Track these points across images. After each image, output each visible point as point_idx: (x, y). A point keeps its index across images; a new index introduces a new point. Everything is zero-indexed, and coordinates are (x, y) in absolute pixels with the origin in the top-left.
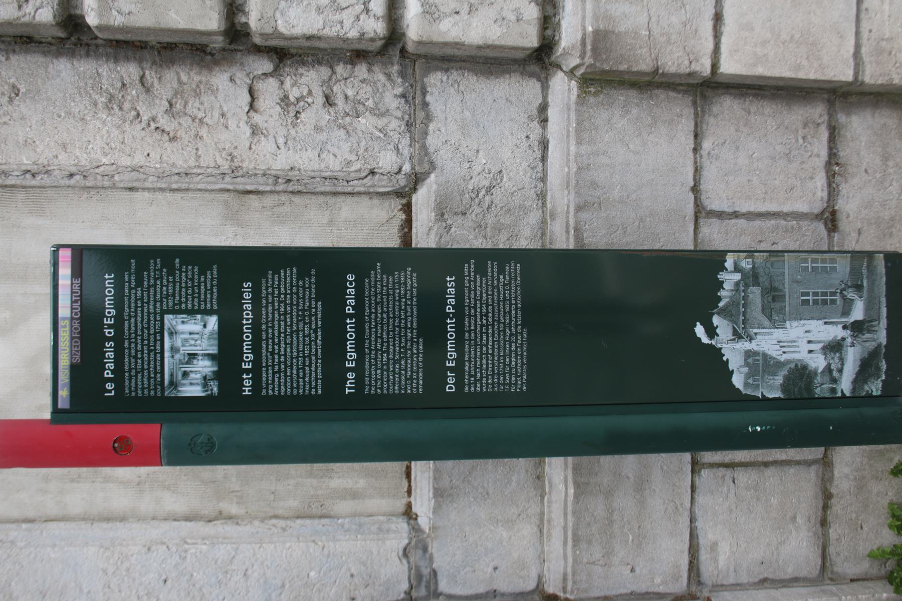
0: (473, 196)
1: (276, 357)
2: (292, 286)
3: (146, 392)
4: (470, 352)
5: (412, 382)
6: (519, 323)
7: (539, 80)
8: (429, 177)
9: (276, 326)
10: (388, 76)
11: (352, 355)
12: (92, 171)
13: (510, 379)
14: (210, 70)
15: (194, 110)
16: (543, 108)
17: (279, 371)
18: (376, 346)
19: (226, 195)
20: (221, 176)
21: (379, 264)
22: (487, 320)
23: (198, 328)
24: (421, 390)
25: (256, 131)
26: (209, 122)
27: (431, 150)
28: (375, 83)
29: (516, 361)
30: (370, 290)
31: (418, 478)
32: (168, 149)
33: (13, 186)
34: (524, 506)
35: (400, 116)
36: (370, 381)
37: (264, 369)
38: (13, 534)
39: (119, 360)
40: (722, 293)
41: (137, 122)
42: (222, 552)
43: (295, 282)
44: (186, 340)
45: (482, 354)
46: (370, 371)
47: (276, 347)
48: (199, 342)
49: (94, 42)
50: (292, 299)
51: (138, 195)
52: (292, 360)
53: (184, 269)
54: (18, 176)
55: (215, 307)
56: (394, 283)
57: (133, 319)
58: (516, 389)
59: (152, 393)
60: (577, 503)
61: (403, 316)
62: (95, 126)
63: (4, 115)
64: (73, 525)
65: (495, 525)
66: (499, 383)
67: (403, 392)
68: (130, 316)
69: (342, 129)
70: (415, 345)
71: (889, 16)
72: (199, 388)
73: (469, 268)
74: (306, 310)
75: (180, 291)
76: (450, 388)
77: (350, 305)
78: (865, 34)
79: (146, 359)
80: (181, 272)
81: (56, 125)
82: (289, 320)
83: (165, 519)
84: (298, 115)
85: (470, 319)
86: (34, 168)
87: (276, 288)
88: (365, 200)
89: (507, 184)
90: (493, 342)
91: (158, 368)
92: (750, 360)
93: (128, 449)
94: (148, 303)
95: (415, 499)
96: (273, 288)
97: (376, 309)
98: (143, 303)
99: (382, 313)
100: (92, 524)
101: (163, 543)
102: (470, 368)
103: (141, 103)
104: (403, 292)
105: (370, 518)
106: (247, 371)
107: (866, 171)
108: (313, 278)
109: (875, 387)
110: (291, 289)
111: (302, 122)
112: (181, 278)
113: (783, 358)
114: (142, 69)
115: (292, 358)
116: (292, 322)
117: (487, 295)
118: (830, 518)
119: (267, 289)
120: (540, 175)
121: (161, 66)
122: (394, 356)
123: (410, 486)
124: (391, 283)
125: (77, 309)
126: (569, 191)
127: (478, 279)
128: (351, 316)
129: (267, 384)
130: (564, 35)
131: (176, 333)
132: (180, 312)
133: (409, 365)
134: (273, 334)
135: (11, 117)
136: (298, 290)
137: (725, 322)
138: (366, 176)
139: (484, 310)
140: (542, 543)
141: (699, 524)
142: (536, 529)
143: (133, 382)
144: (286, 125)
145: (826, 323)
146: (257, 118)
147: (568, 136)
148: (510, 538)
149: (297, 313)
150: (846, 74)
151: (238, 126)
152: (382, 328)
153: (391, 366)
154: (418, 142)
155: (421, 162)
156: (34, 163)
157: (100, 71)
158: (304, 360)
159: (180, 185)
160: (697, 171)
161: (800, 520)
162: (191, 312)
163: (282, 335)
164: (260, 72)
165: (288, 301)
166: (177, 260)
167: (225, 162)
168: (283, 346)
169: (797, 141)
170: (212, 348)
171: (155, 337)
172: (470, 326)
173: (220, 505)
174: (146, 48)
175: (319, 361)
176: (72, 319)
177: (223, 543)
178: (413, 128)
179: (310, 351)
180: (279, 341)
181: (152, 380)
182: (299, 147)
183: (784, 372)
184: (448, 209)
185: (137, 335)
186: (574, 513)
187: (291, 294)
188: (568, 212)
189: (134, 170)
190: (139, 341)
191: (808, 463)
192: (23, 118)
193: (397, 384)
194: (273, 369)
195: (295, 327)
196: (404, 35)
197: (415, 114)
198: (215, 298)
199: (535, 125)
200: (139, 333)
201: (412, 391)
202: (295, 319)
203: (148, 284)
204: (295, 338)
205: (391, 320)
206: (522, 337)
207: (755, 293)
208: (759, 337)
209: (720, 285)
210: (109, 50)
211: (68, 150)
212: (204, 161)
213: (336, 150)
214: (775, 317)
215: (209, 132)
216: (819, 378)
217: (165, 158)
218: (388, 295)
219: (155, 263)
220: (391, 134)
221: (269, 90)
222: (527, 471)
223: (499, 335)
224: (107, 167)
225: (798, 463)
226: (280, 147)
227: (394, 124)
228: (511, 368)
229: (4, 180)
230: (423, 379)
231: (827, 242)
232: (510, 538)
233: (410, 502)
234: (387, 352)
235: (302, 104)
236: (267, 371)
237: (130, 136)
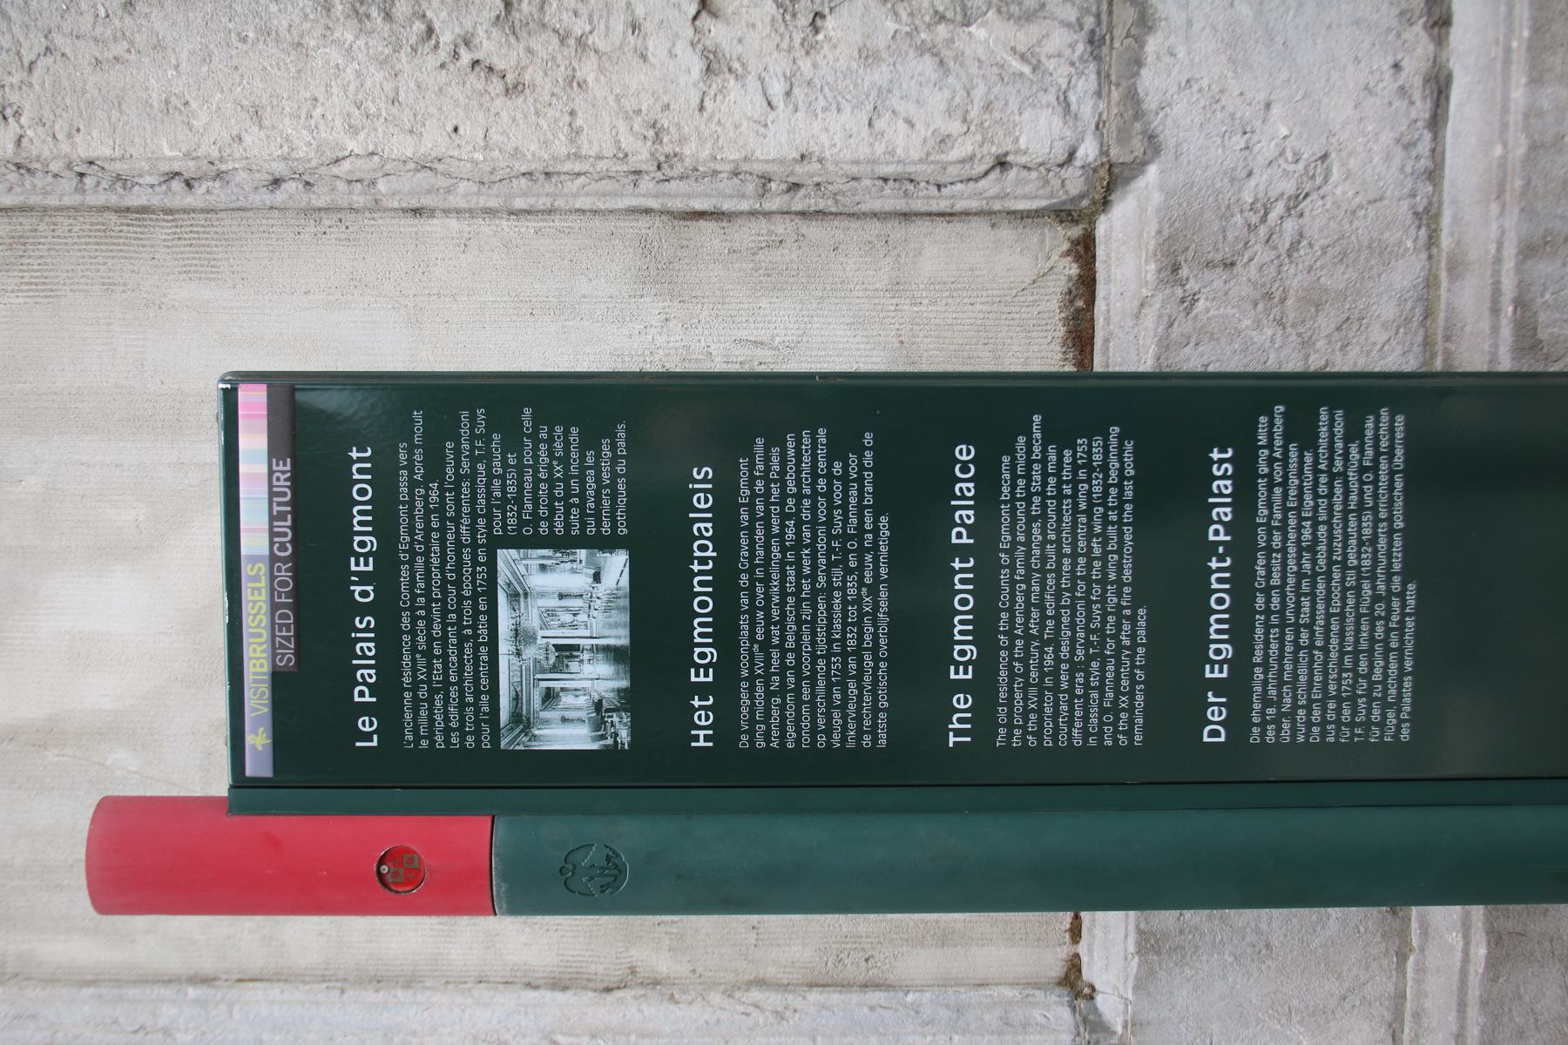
0: (1254, 219)
1: (775, 655)
2: (815, 475)
4: (1267, 643)
5: (1117, 719)
8: (1143, 172)
9: (775, 576)
12: (323, 170)
13: (1369, 710)
15: (565, 17)
18: (1027, 629)
19: (643, 222)
20: (631, 177)
21: (1037, 419)
22: (1314, 562)
23: (581, 582)
24: (1138, 738)
25: (715, 66)
27: (1150, 103)
29: (1386, 667)
30: (1014, 486)
32: (504, 114)
33: (144, 210)
34: (1357, 977)
35: (1073, 19)
36: (1010, 715)
37: (744, 685)
38: (168, 1013)
39: (387, 662)
41: (427, 49)
43: (822, 465)
44: (551, 613)
45: (1298, 648)
46: (1011, 692)
47: (775, 631)
48: (582, 617)
50: (814, 509)
51: (434, 226)
52: (814, 663)
53: (544, 435)
54: (152, 186)
55: (623, 530)
56: (1075, 468)
57: (420, 560)
58: (1381, 737)
60: (1495, 980)
61: (1097, 551)
62: (327, 62)
63: (115, 39)
65: (1283, 1020)
66: (1338, 723)
67: (1092, 742)
68: (413, 554)
69: (927, 56)
73: (1270, 428)
74: (851, 537)
75: (536, 489)
77: (963, 525)
79: (454, 658)
80: (537, 441)
81: (235, 63)
82: (806, 562)
84: (819, 22)
85: (1269, 558)
86: (190, 169)
87: (775, 481)
88: (980, 227)
89: (1340, 188)
90: (1328, 616)
91: (484, 681)
93: (414, 878)
94: (457, 520)
95: (1090, 951)
96: (768, 481)
97: (1028, 533)
98: (443, 519)
99: (1043, 545)
100: (342, 991)
102: (1265, 683)
104: (1097, 489)
105: (982, 991)
106: (703, 690)
108: (868, 454)
110: (813, 485)
111: (828, 39)
112: (536, 457)
115: (814, 658)
116: (814, 567)
117: (1316, 496)
119: (751, 485)
120: (1425, 163)
122: (1073, 652)
124: (1067, 467)
125: (285, 535)
126: (1503, 206)
127: (1293, 455)
128: (963, 552)
129: (752, 721)
131: (526, 595)
134: (768, 598)
135: (132, 43)
136: (830, 485)
138: (986, 173)
139: (1307, 534)
142: (1382, 1032)
143: (423, 713)
146: (717, 32)
147: (1507, 62)
149: (828, 543)
151: (671, 54)
153: (1064, 678)
154: (1118, 85)
155: (1124, 135)
156: (187, 155)
158: (845, 663)
159: (532, 200)
162: (564, 543)
163: (791, 600)
166: (527, 411)
167: (640, 143)
170: (614, 632)
171: (475, 606)
172: (1268, 577)
173: (633, 952)
175: (883, 665)
176: (273, 559)
178: (1105, 50)
179: (860, 639)
180: (783, 615)
181: (469, 710)
182: (822, 102)
184: (1190, 253)
185: (430, 600)
186: (1484, 1003)
188: (1498, 260)
190: (436, 615)
192: (158, 46)
194: (767, 684)
195: (822, 579)
197: (1110, 13)
198: (622, 506)
200: (436, 593)
201: (1116, 740)
203: (456, 473)
204: (822, 607)
205: (1066, 561)
206: (1404, 606)
211: (266, 123)
212: (590, 142)
215: (601, 70)
217: (495, 137)
218: (1060, 497)
220: (1051, 65)
223: (1344, 599)
224: (359, 162)
226: (775, 102)
227: (1059, 39)
228: (1371, 684)
229: (122, 197)
230: (1145, 711)
233: (1077, 956)
234: (1056, 642)
236: (752, 690)
237: (412, 85)
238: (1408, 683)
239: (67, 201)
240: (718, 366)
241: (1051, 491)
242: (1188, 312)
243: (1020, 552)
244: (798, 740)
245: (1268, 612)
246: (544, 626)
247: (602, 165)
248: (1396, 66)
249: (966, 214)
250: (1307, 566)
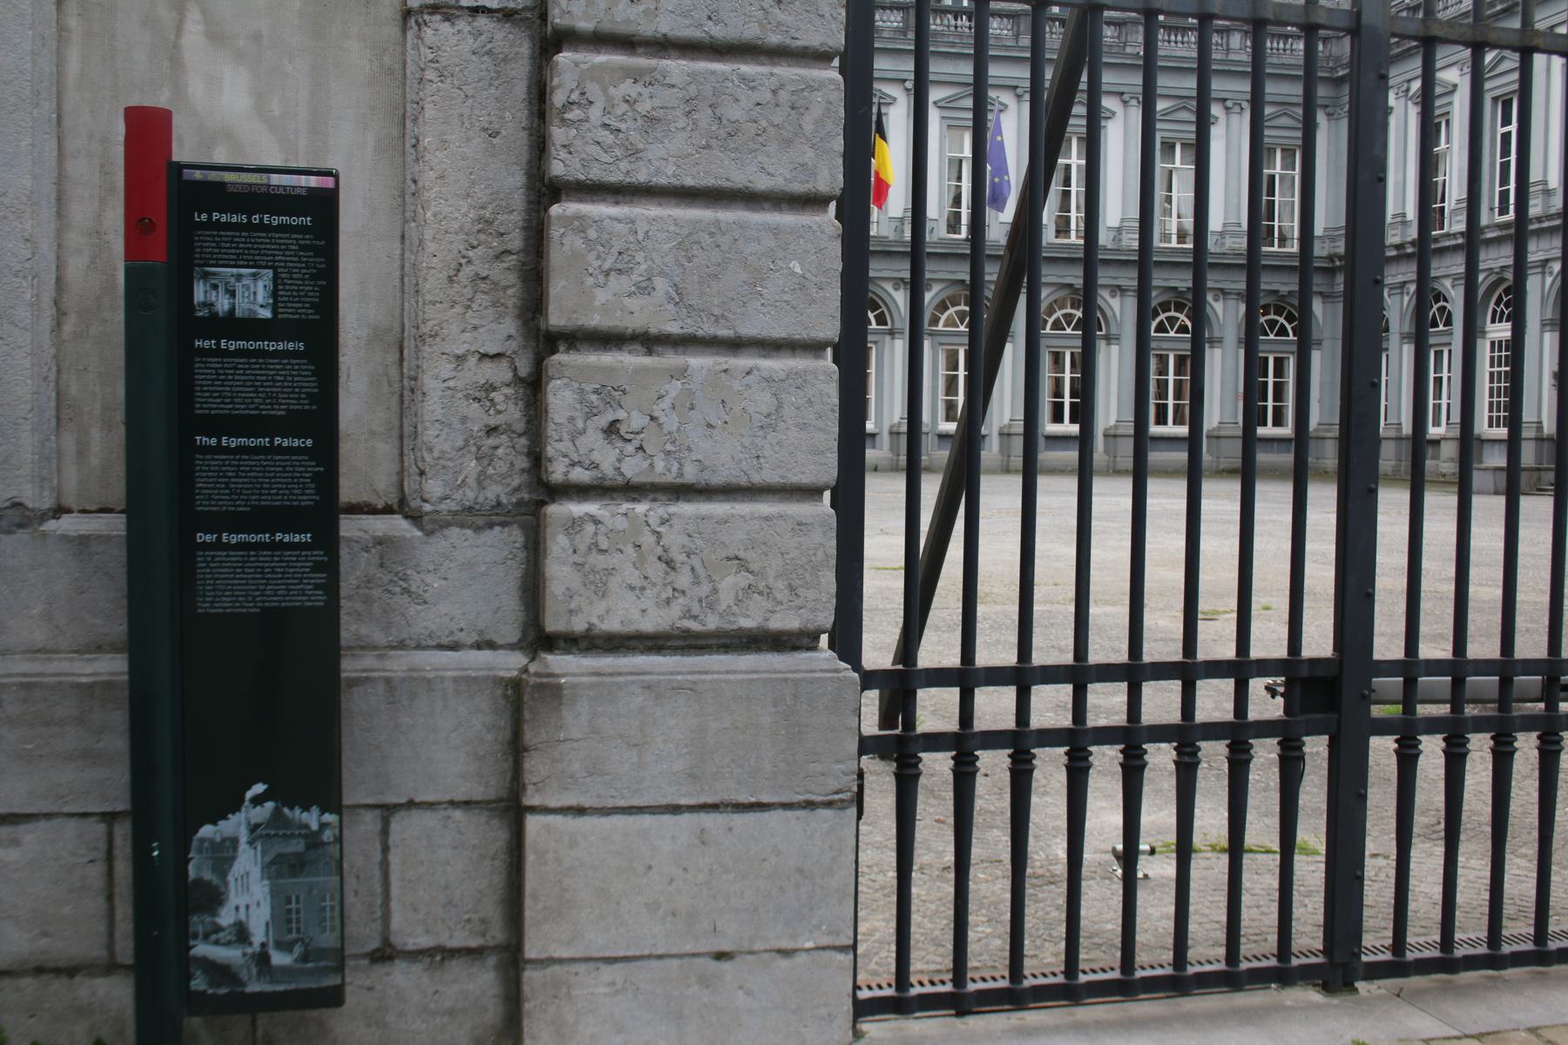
1: (232, 372)
2: (301, 387)
3: (198, 250)
6: (266, 604)
7: (520, 641)
9: (263, 372)
10: (517, 489)
11: (234, 443)
14: (519, 316)
16: (491, 645)
17: (218, 374)
18: (242, 466)
19: (398, 329)
21: (322, 469)
22: (269, 573)
23: (260, 299)
26: (468, 315)
27: (446, 532)
28: (511, 476)
30: (297, 461)
31: (99, 520)
33: (404, 125)
40: (297, 811)
42: (23, 314)
44: (248, 289)
45: (235, 568)
47: (241, 372)
48: (246, 300)
49: (542, 208)
50: (288, 387)
51: (397, 244)
55: (280, 316)
56: (304, 483)
57: (268, 241)
59: (197, 256)
61: (272, 492)
64: (54, 164)
70: (243, 503)
71: (592, 994)
72: (202, 298)
73: (319, 556)
76: (201, 537)
78: (574, 968)
80: (313, 286)
82: (268, 384)
83: (58, 257)
86: (420, 148)
88: (395, 468)
89: (413, 609)
91: (222, 262)
92: (227, 843)
94: (283, 255)
97: (279, 466)
101: (34, 254)
102: (220, 556)
103: (484, 250)
104: (296, 491)
106: (218, 344)
107: (436, 992)
109: (199, 983)
113: (231, 878)
114: (517, 253)
116: (266, 387)
117: (294, 573)
118: (45, 977)
121: (521, 270)
123: (91, 512)
128: (272, 442)
129: (205, 362)
130: (559, 657)
132: (275, 284)
133: (224, 497)
137: (268, 815)
138: (418, 467)
139: (279, 570)
140: (24, 652)
141: (43, 824)
143: (208, 239)
144: (466, 389)
145: (267, 924)
146: (473, 360)
148: (31, 617)
150: (531, 952)
151: (465, 342)
152: (260, 472)
153: (223, 480)
155: (433, 521)
156: (425, 148)
157: (515, 213)
160: (431, 806)
161: (43, 942)
162: (275, 294)
164: (517, 364)
165: (286, 384)
166: (325, 283)
168: (243, 378)
169: (466, 913)
174: (538, 256)
176: (269, 186)
177: (32, 315)
179: (238, 404)
180: (248, 375)
181: (210, 256)
183: (216, 881)
186: (60, 683)
187: (292, 387)
188: (385, 670)
189: (421, 241)
191: (110, 945)
192: (468, 140)
193: (205, 485)
194: (221, 368)
195: (261, 389)
196: (554, 501)
199: (474, 637)
200: (256, 246)
202: (268, 390)
204: (251, 389)
205: (267, 480)
206: (252, 607)
207: (298, 846)
208: (252, 852)
209: (306, 808)
210: (535, 222)
213: (442, 438)
214: (273, 868)
215: (459, 314)
216: (208, 919)
217: (432, 271)
218: (293, 478)
219: (322, 263)
221: (499, 373)
222: (106, 635)
225: (111, 935)
227: (471, 495)
231: (359, 952)
232: (31, 617)
235: (488, 404)
238: (221, 611)
239: (408, 95)
240: (341, 359)
241: (295, 474)
242: (362, 549)
243: (272, 463)
244: (198, 380)
245: (249, 556)
246: (243, 286)
247: (421, 313)
248: (462, 630)
249: (402, 461)
250: (267, 570)
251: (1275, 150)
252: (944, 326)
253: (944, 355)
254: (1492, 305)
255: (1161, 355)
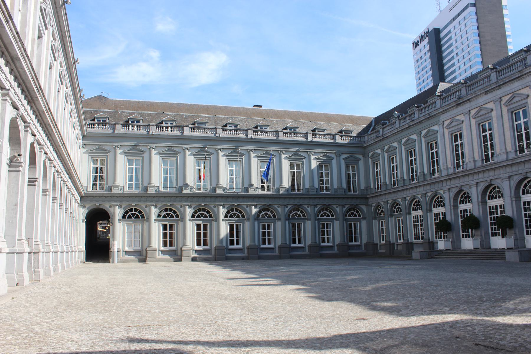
251: (349, 166)
252: (348, 217)
253: (262, 226)
254: (459, 198)
255: (293, 224)
